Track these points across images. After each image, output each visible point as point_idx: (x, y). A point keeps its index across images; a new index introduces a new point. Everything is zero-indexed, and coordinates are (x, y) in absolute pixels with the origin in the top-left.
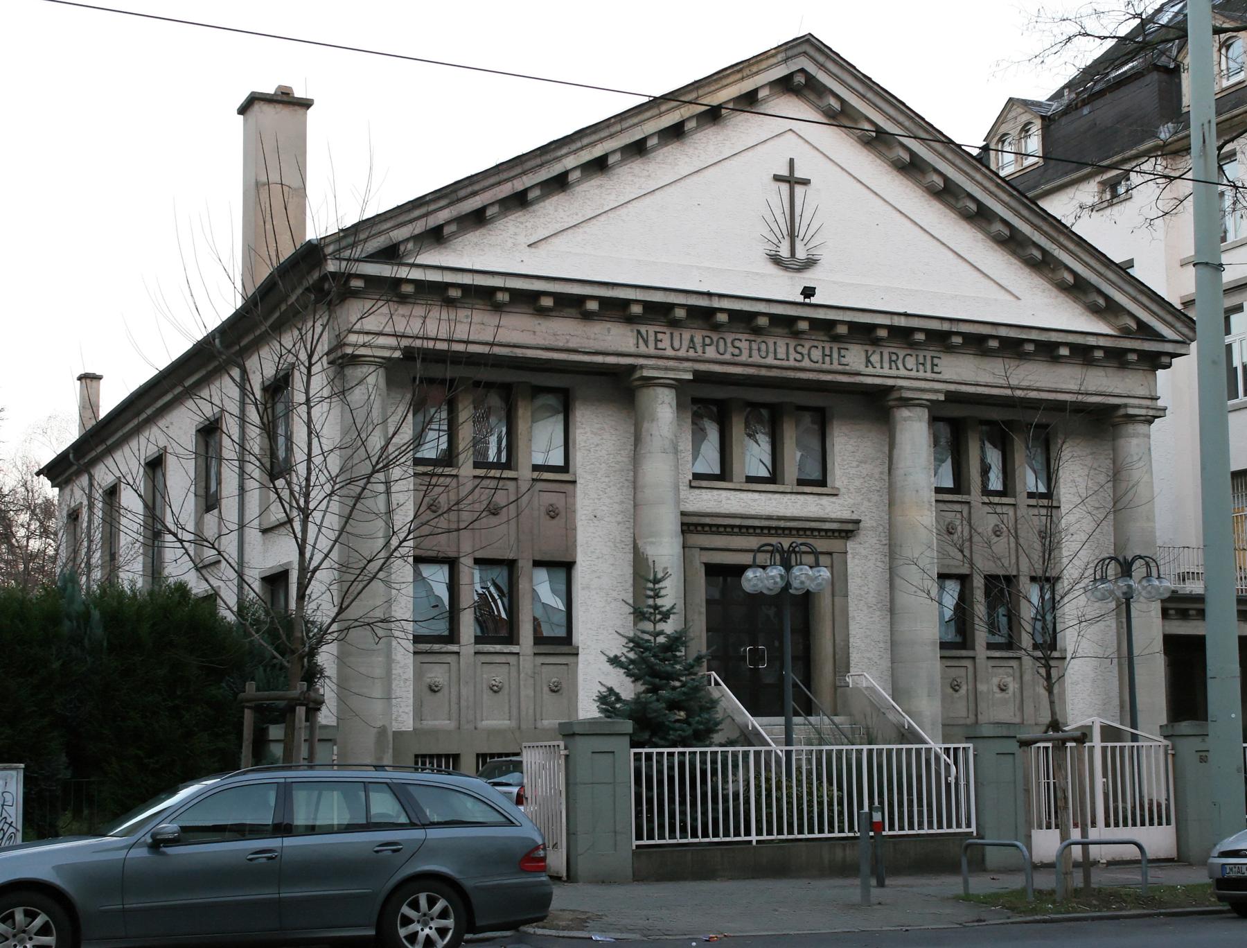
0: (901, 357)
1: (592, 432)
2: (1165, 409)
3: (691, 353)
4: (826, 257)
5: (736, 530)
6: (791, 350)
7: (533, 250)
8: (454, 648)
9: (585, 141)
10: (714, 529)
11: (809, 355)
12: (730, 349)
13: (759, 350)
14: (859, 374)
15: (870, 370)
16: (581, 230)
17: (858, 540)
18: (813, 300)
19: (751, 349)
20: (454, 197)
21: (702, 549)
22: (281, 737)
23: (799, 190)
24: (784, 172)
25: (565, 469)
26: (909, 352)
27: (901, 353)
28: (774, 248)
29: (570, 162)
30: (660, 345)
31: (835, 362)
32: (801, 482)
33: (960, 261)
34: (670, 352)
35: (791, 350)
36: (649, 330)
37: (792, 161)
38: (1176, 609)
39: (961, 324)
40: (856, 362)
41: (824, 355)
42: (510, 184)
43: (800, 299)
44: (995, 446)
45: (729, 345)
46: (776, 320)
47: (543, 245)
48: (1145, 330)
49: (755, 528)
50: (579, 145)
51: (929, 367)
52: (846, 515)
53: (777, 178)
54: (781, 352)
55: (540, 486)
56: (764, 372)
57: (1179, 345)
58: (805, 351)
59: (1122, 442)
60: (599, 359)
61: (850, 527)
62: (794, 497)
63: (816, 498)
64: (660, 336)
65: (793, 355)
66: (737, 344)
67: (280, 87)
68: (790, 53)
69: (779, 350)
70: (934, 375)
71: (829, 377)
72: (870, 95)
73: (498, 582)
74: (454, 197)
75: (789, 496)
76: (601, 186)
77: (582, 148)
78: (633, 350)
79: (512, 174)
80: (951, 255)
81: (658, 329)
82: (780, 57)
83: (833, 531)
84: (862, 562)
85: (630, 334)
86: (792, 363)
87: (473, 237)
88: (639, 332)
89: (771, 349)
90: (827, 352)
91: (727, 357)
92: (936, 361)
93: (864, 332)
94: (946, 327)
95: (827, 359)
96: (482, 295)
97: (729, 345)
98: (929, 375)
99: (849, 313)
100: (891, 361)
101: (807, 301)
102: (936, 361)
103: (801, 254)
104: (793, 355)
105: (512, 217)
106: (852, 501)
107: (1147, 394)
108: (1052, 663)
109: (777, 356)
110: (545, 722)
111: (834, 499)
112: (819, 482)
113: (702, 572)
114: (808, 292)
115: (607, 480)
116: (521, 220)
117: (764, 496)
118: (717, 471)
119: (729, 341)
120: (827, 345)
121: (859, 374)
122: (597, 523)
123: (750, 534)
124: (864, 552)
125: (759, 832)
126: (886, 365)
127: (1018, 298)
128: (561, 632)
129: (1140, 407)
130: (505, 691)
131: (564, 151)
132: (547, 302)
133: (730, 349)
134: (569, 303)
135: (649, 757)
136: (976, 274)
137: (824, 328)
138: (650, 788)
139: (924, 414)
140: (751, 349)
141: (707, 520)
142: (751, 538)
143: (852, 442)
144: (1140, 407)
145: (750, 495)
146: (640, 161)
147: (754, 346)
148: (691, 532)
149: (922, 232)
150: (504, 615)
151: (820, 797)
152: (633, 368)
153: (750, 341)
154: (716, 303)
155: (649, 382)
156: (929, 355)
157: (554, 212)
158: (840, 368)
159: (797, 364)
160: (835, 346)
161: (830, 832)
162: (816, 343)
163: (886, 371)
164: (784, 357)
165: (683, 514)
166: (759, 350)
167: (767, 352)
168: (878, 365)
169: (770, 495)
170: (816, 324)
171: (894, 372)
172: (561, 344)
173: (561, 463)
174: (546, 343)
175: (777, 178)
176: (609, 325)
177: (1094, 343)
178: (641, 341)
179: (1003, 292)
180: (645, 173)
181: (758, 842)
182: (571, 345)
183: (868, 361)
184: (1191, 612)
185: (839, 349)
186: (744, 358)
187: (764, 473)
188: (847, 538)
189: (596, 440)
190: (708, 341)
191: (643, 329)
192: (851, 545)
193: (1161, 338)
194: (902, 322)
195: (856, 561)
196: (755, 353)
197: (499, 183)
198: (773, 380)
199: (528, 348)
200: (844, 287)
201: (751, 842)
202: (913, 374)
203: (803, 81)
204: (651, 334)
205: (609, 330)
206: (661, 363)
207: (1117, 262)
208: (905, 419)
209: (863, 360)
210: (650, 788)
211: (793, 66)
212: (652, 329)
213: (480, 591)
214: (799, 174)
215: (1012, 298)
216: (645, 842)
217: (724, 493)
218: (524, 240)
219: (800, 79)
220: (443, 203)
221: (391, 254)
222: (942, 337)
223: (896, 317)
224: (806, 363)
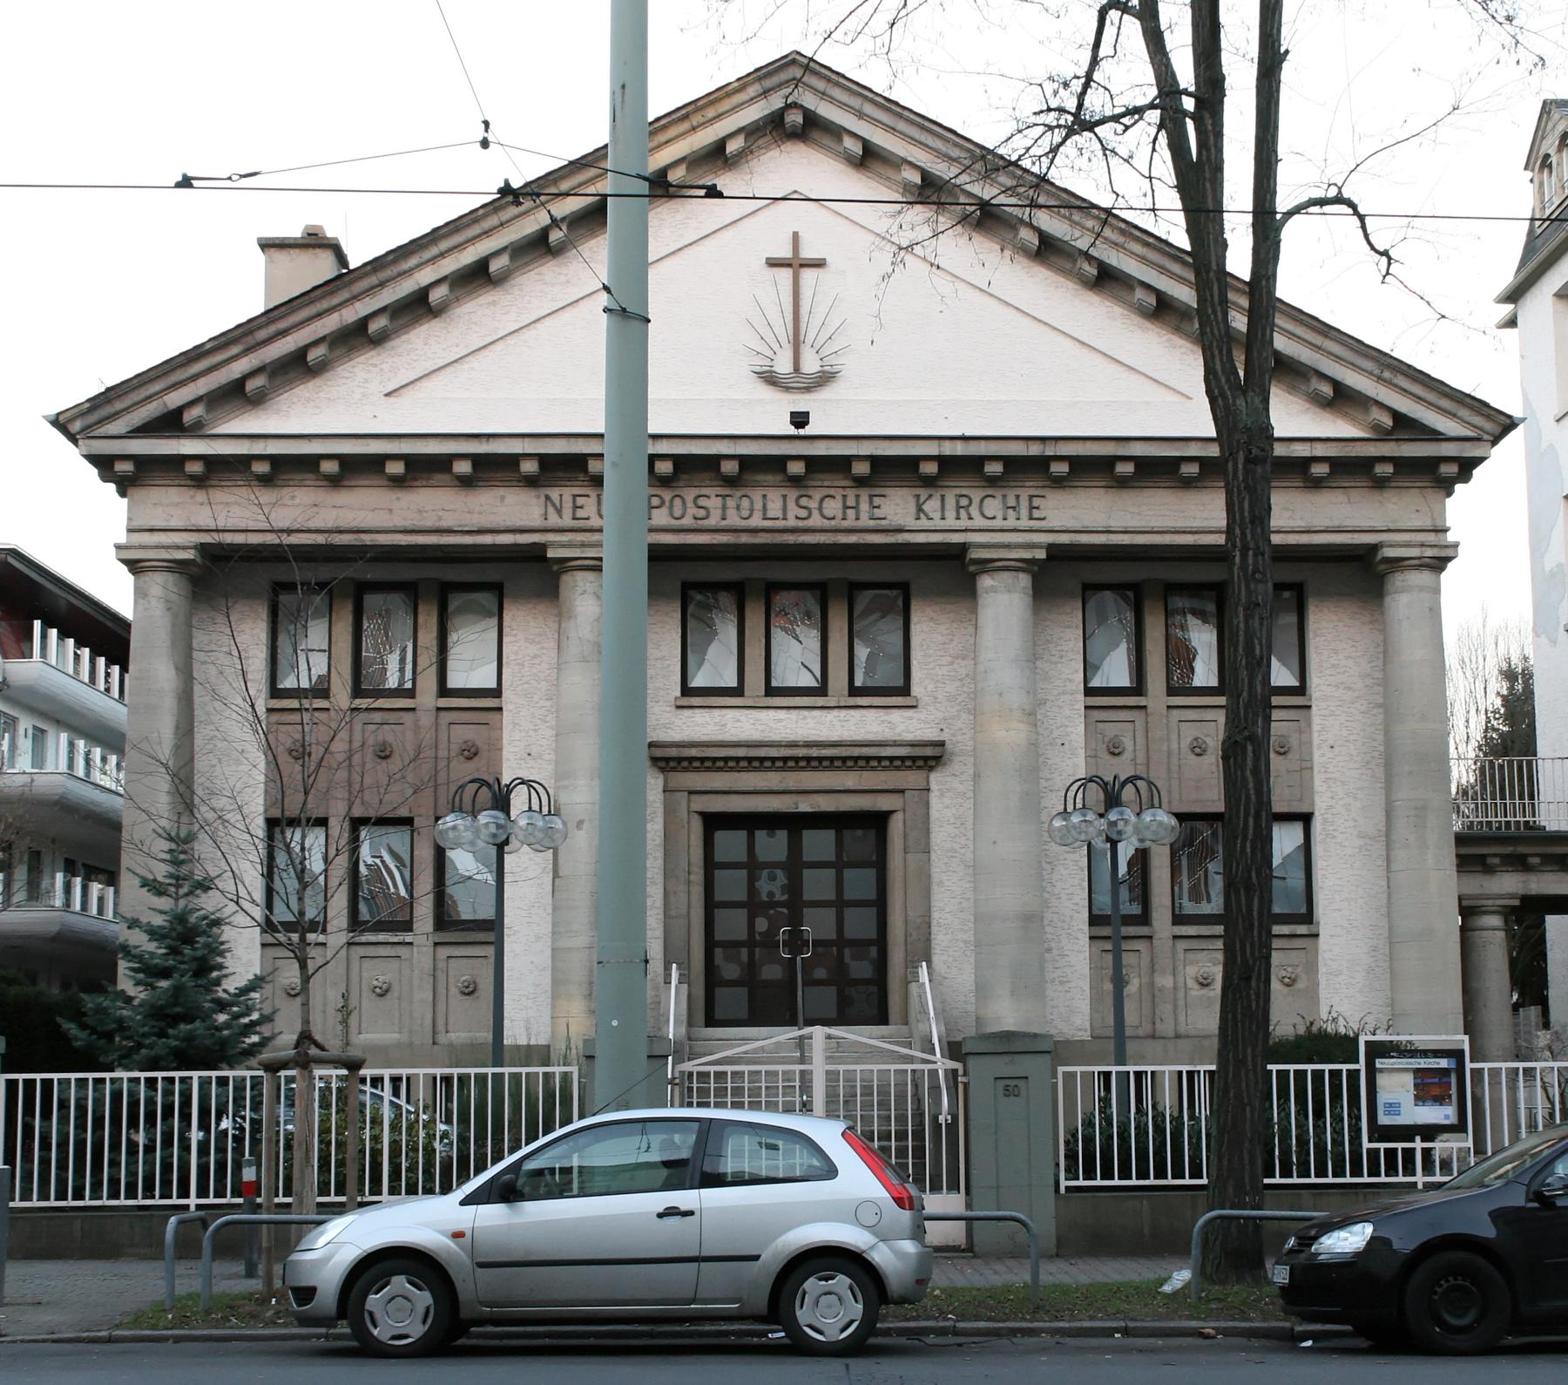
0: (976, 501)
1: (527, 640)
2: (1456, 546)
4: (850, 366)
5: (744, 764)
6: (791, 505)
7: (391, 399)
8: (1143, 930)
9: (444, 245)
10: (707, 764)
11: (820, 509)
12: (692, 511)
13: (738, 508)
14: (900, 530)
15: (924, 523)
16: (466, 366)
17: (949, 770)
19: (724, 508)
20: (250, 340)
21: (691, 793)
23: (808, 275)
24: (785, 252)
25: (497, 693)
26: (990, 491)
27: (976, 495)
28: (768, 362)
29: (425, 277)
30: (580, 513)
31: (864, 516)
32: (854, 691)
33: (1086, 350)
35: (791, 505)
36: (563, 494)
37: (796, 236)
38: (1502, 856)
39: (1061, 444)
40: (901, 514)
41: (846, 507)
42: (336, 315)
43: (792, 431)
44: (1205, 621)
45: (690, 504)
46: (750, 464)
47: (408, 394)
48: (1404, 425)
49: (773, 760)
51: (1024, 512)
52: (931, 734)
53: (773, 263)
54: (775, 508)
55: (447, 717)
56: (745, 539)
57: (1468, 445)
58: (813, 504)
59: (1388, 600)
60: (487, 539)
61: (929, 752)
62: (843, 713)
63: (881, 712)
64: (580, 501)
65: (793, 510)
66: (702, 502)
67: (307, 227)
68: (768, 83)
69: (770, 505)
70: (1033, 524)
71: (852, 539)
72: (902, 126)
73: (397, 848)
74: (250, 340)
75: (835, 712)
76: (494, 303)
77: (442, 255)
78: (537, 522)
79: (335, 300)
80: (1068, 343)
81: (577, 491)
82: (752, 91)
83: (902, 759)
84: (947, 798)
85: (534, 501)
86: (792, 522)
87: (305, 391)
88: (547, 498)
89: (758, 505)
90: (851, 502)
91: (687, 521)
92: (1036, 502)
93: (893, 468)
94: (1035, 450)
95: (851, 513)
96: (289, 468)
97: (690, 504)
98: (1025, 523)
99: (866, 443)
100: (959, 507)
101: (802, 432)
103: (810, 365)
104: (793, 510)
105: (362, 359)
106: (940, 715)
107: (1428, 524)
108: (1125, 945)
109: (768, 512)
110: (452, 1036)
111: (910, 713)
112: (900, 690)
114: (800, 419)
115: (548, 704)
116: (374, 361)
117: (794, 714)
118: (774, 684)
119: (689, 499)
120: (851, 493)
121: (900, 530)
122: (531, 763)
123: (768, 769)
124: (961, 788)
125: (202, 1192)
126: (950, 514)
127: (1189, 398)
128: (487, 913)
129: (1408, 545)
130: (395, 993)
131: (413, 261)
132: (1320, 470)
133: (692, 511)
134: (423, 467)
135: (222, 1082)
136: (1113, 367)
137: (828, 467)
138: (81, 1126)
139: (1024, 580)
140: (724, 508)
141: (694, 752)
142: (771, 774)
143: (942, 628)
144: (1408, 545)
145: (772, 713)
146: (554, 262)
147: (731, 503)
148: (674, 769)
149: (1019, 315)
150: (403, 892)
152: (1375, 548)
153: (724, 497)
156: (1024, 494)
157: (423, 345)
158: (872, 523)
159: (801, 524)
160: (864, 494)
161: (110, 1197)
162: (832, 492)
163: (951, 522)
164: (780, 514)
165: (651, 745)
166: (738, 508)
167: (752, 511)
168: (937, 515)
169: (805, 713)
170: (817, 465)
171: (964, 523)
172: (429, 523)
174: (408, 524)
175: (773, 263)
176: (501, 491)
177: (1307, 454)
178: (551, 510)
179: (1162, 390)
180: (563, 278)
181: (199, 1207)
182: (444, 524)
183: (920, 509)
184: (1490, 861)
185: (871, 497)
186: (713, 521)
187: (807, 680)
188: (931, 769)
189: (533, 649)
190: (964, 502)
191: (554, 493)
192: (936, 779)
193: (1435, 436)
194: (959, 449)
195: (947, 801)
196: (731, 513)
197: (319, 315)
198: (805, 549)
199: (378, 532)
200: (866, 406)
201: (187, 1207)
202: (998, 523)
203: (800, 119)
204: (568, 500)
205: (503, 498)
206: (580, 537)
208: (993, 589)
209: (912, 508)
211: (776, 102)
212: (567, 493)
213: (370, 861)
214: (807, 253)
215: (1177, 398)
216: (1400, 1146)
217: (730, 713)
218: (378, 386)
219: (795, 118)
220: (235, 350)
221: (170, 423)
222: (1030, 466)
223: (947, 443)
224: (816, 521)
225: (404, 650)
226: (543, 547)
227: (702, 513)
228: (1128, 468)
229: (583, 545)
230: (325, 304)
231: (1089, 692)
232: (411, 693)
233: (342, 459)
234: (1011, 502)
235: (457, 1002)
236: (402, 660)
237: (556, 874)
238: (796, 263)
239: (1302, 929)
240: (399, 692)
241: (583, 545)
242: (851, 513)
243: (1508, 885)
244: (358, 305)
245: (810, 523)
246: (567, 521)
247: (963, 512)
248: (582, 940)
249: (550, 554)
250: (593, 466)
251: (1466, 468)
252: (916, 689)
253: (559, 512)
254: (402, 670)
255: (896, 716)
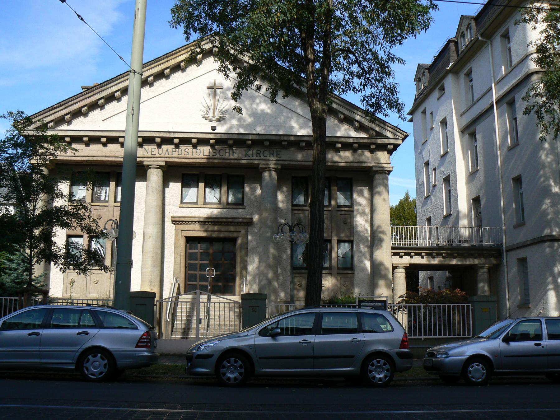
0: (262, 152)
3: (167, 155)
12: (184, 153)
18: (216, 131)
22: (206, 300)
27: (262, 150)
34: (157, 155)
43: (212, 131)
50: (117, 82)
56: (198, 161)
66: (186, 150)
77: (119, 83)
87: (82, 119)
91: (182, 156)
92: (278, 153)
102: (278, 153)
113: (184, 240)
125: (425, 335)
129: (150, 161)
144: (150, 161)
151: (430, 322)
154: (172, 135)
155: (148, 167)
172: (112, 155)
173: (185, 201)
174: (107, 155)
182: (116, 155)
186: (189, 156)
190: (259, 152)
207: (309, 108)
210: (444, 314)
216: (428, 337)
225: (106, 193)
226: (142, 162)
227: (187, 153)
228: (286, 143)
229: (154, 161)
230: (87, 96)
231: (293, 205)
232: (107, 202)
233: (198, 139)
234: (272, 152)
235: (92, 285)
236: (106, 193)
237: (143, 251)
238: (215, 87)
239: (350, 272)
240: (105, 201)
241: (154, 161)
242: (227, 154)
243: (407, 261)
244: (96, 96)
245: (216, 157)
246: (150, 155)
247: (258, 155)
248: (149, 270)
249: (145, 163)
250: (121, 140)
251: (396, 146)
252: (245, 204)
253: (148, 153)
254: (106, 196)
255: (240, 211)
